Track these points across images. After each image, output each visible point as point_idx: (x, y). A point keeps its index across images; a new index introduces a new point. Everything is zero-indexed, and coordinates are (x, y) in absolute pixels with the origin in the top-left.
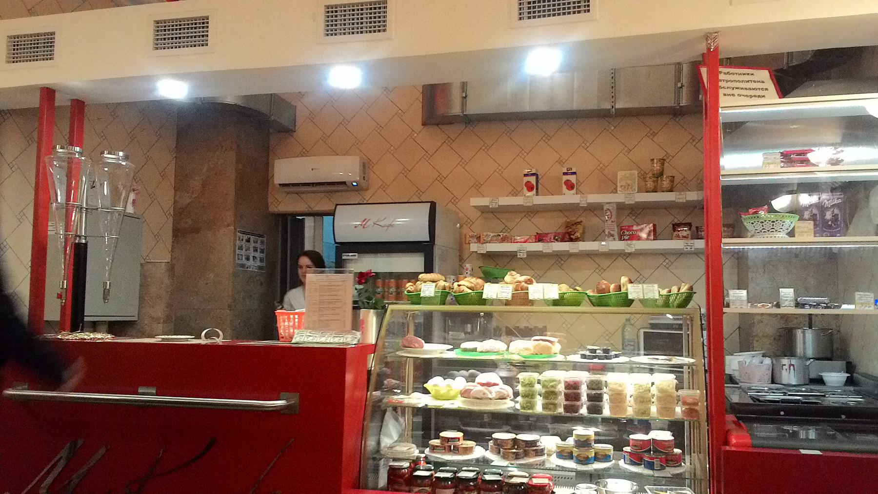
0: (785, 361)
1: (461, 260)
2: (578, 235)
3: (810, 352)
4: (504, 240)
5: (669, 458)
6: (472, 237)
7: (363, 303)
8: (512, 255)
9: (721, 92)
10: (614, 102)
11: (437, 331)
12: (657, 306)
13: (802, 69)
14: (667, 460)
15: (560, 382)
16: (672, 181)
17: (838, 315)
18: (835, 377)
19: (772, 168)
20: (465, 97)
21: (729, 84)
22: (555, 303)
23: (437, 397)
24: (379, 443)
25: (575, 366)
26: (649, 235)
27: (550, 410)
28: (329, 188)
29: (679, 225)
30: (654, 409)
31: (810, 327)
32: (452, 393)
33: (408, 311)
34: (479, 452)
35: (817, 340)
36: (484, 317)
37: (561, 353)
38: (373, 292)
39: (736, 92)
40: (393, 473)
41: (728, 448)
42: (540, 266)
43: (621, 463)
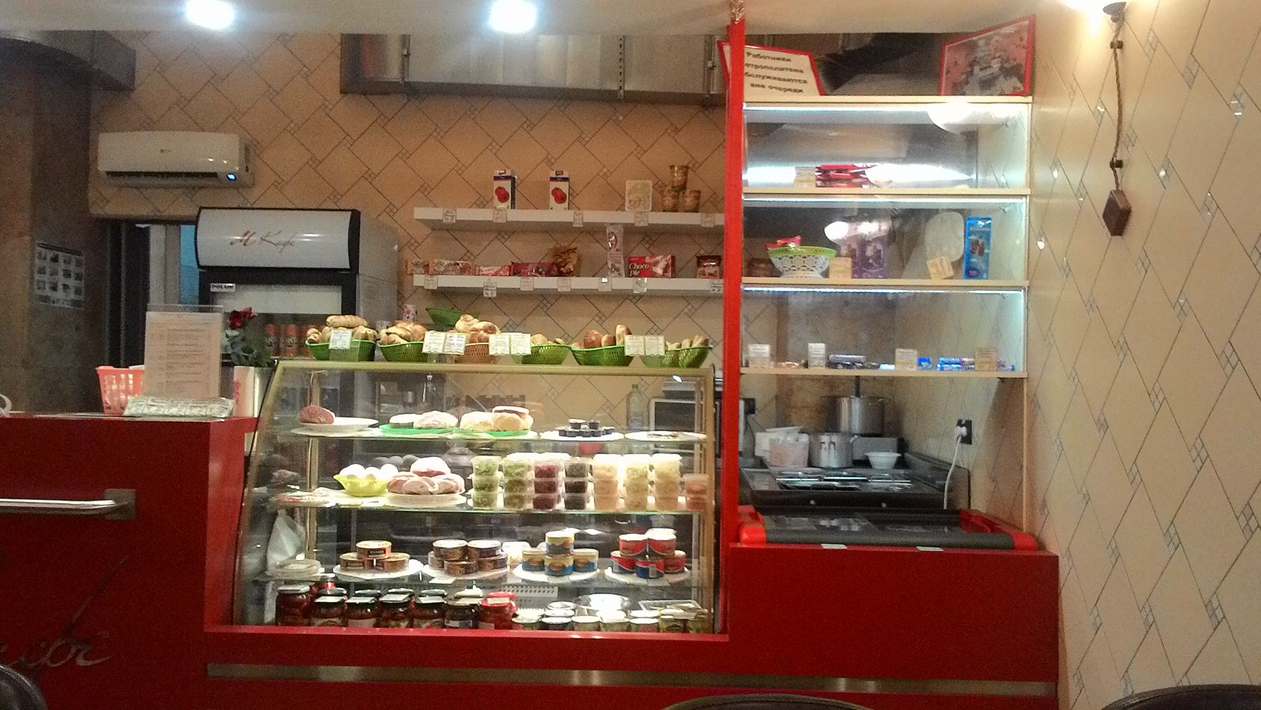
0: (825, 438)
1: (401, 298)
2: (570, 267)
3: (857, 426)
4: (463, 271)
5: (670, 562)
6: (416, 264)
7: (239, 357)
8: (476, 294)
9: (747, 81)
10: (623, 81)
11: (361, 402)
12: (663, 366)
13: (852, 61)
14: (666, 567)
15: (529, 468)
16: (698, 198)
17: (874, 378)
18: (883, 458)
19: (807, 188)
20: (408, 56)
21: (759, 72)
22: (526, 360)
23: (353, 494)
24: (264, 561)
25: (556, 447)
26: (665, 270)
27: (514, 505)
28: (191, 182)
29: (705, 258)
30: (651, 500)
31: (858, 395)
32: (377, 487)
33: (310, 370)
34: (414, 567)
35: (866, 412)
36: (432, 381)
37: (533, 429)
38: (255, 342)
39: (767, 82)
40: (286, 603)
41: (739, 545)
42: (509, 309)
43: (609, 572)
